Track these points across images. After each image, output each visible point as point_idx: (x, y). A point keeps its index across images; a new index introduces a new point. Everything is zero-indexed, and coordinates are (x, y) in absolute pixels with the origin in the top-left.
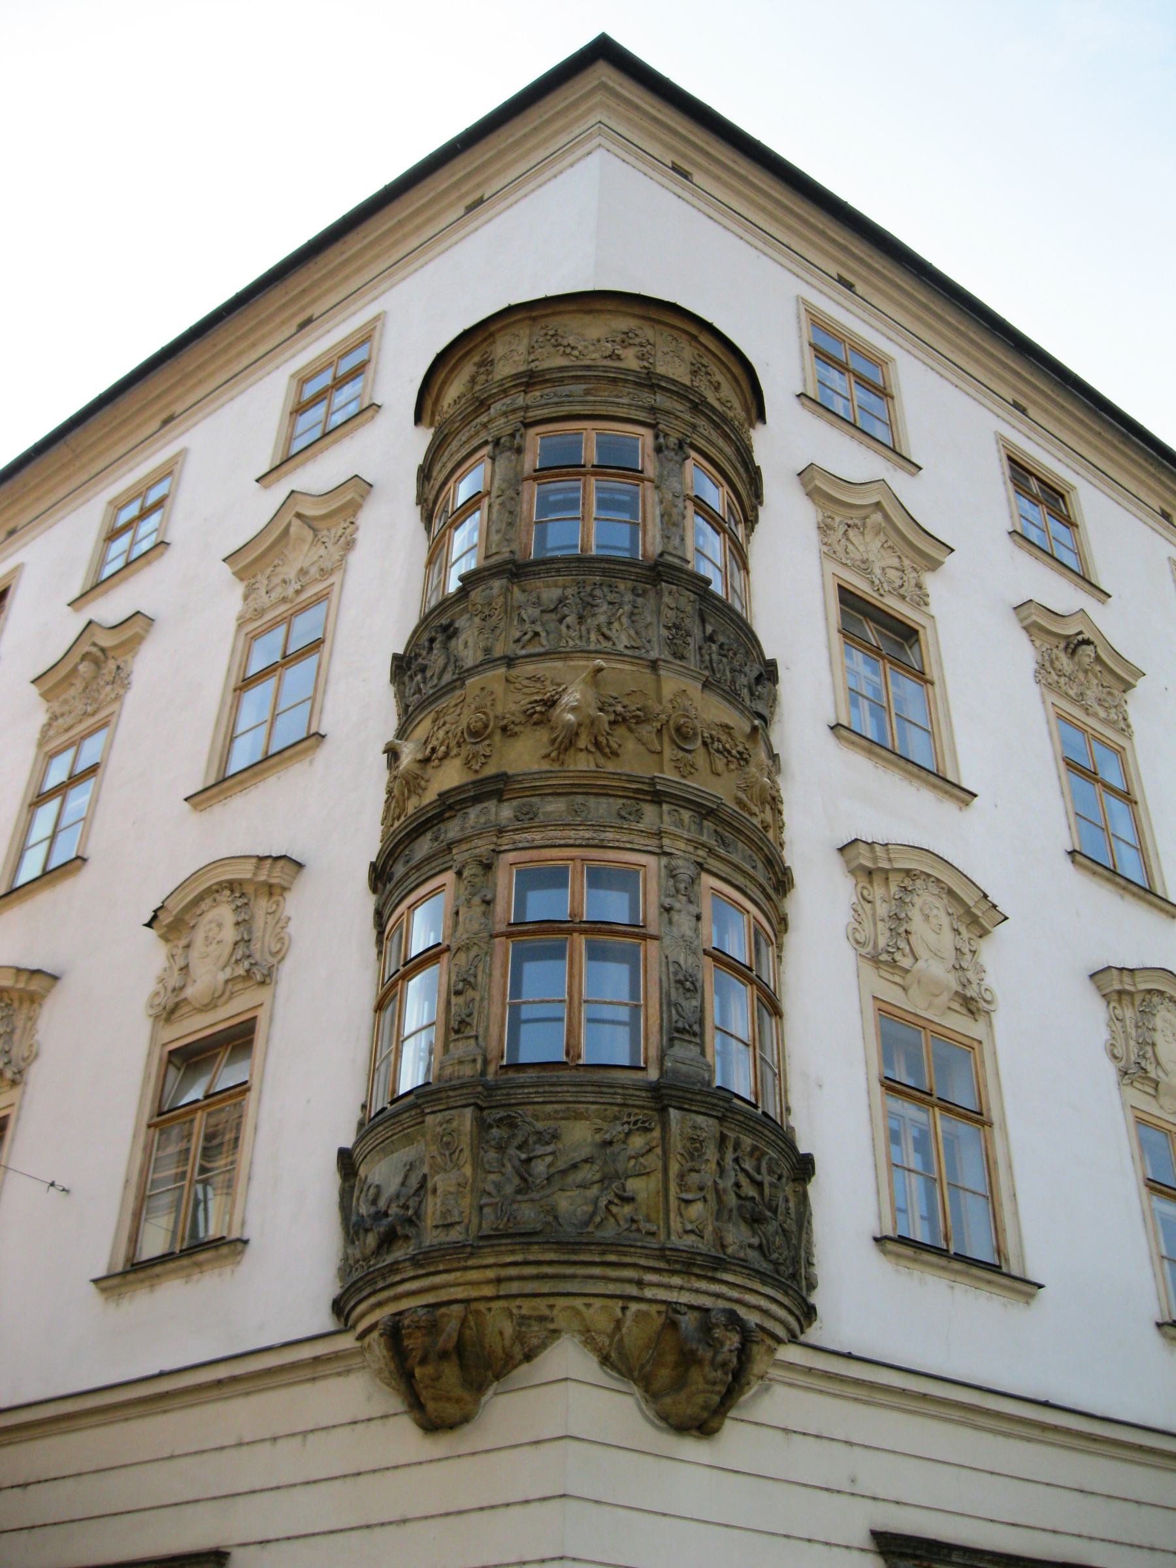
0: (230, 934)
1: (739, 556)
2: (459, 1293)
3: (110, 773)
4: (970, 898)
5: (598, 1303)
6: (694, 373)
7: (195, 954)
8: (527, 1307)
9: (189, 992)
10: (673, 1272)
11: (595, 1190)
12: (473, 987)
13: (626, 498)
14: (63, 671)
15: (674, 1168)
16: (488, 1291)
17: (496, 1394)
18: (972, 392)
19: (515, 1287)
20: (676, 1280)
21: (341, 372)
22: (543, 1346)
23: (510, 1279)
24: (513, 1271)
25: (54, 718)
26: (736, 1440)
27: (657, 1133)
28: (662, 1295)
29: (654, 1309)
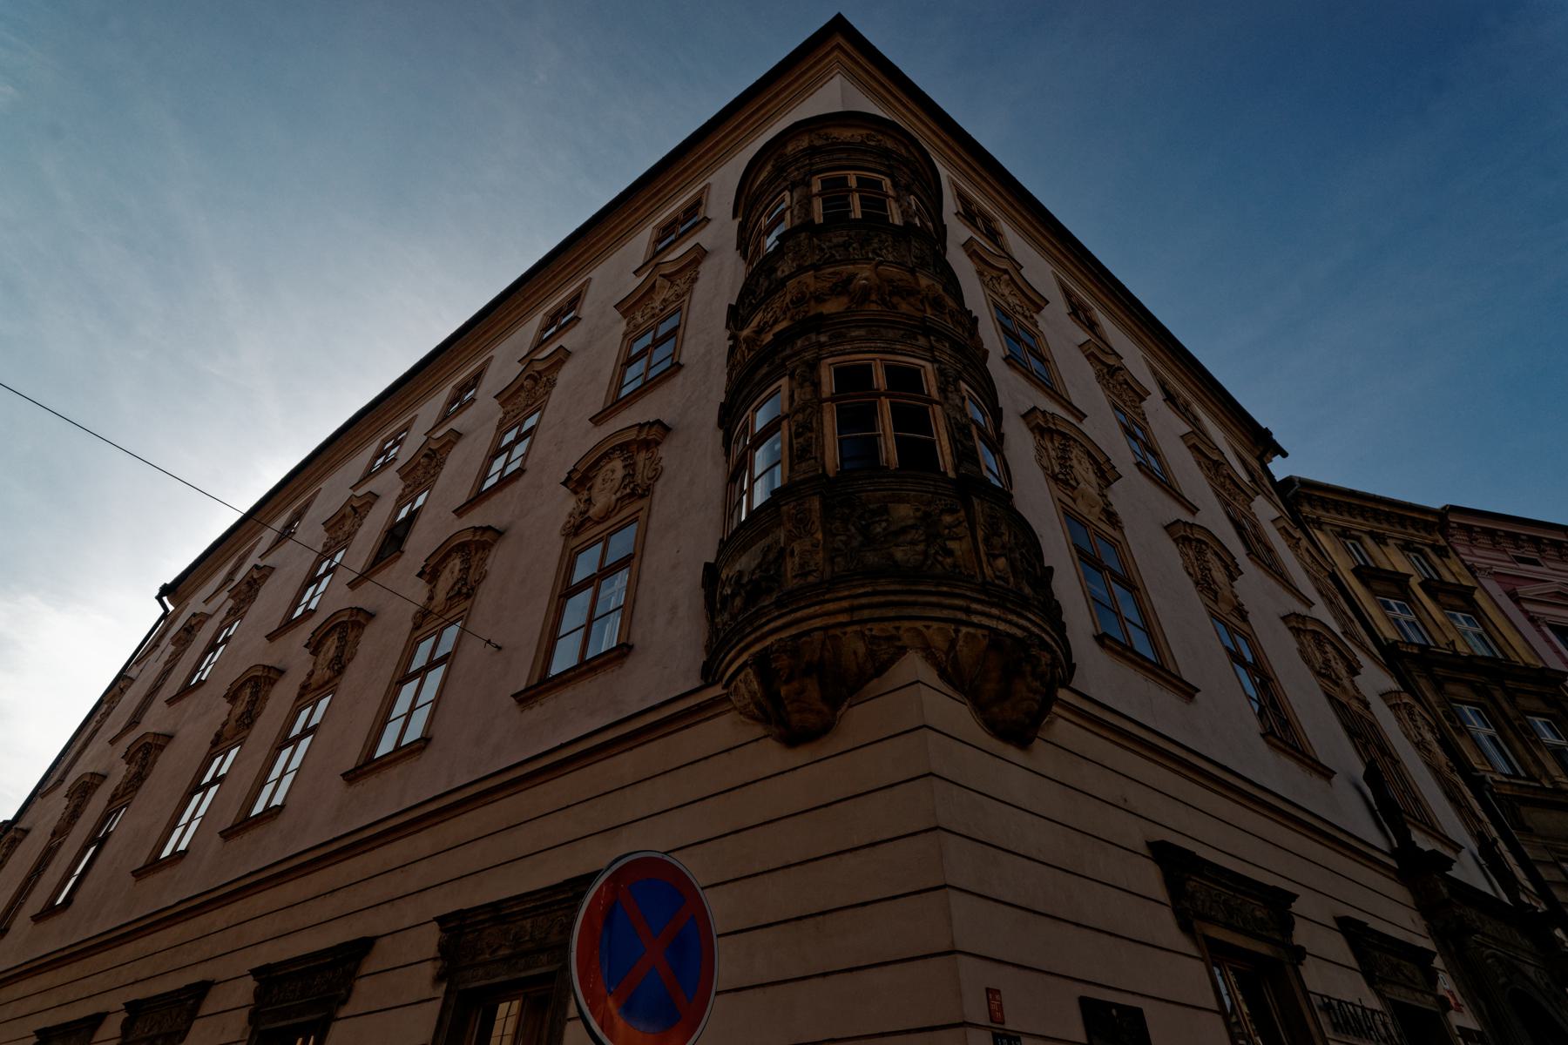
0: (620, 473)
2: (818, 623)
3: (541, 436)
4: (1101, 460)
5: (935, 625)
7: (595, 491)
8: (876, 629)
9: (591, 513)
10: (992, 605)
11: (921, 547)
12: (811, 430)
14: (513, 389)
15: (980, 534)
16: (842, 618)
17: (850, 706)
19: (866, 614)
20: (995, 611)
21: (659, 335)
22: (892, 661)
23: (862, 607)
24: (864, 601)
25: (506, 414)
26: (1042, 755)
27: (962, 513)
28: (986, 621)
29: (980, 632)
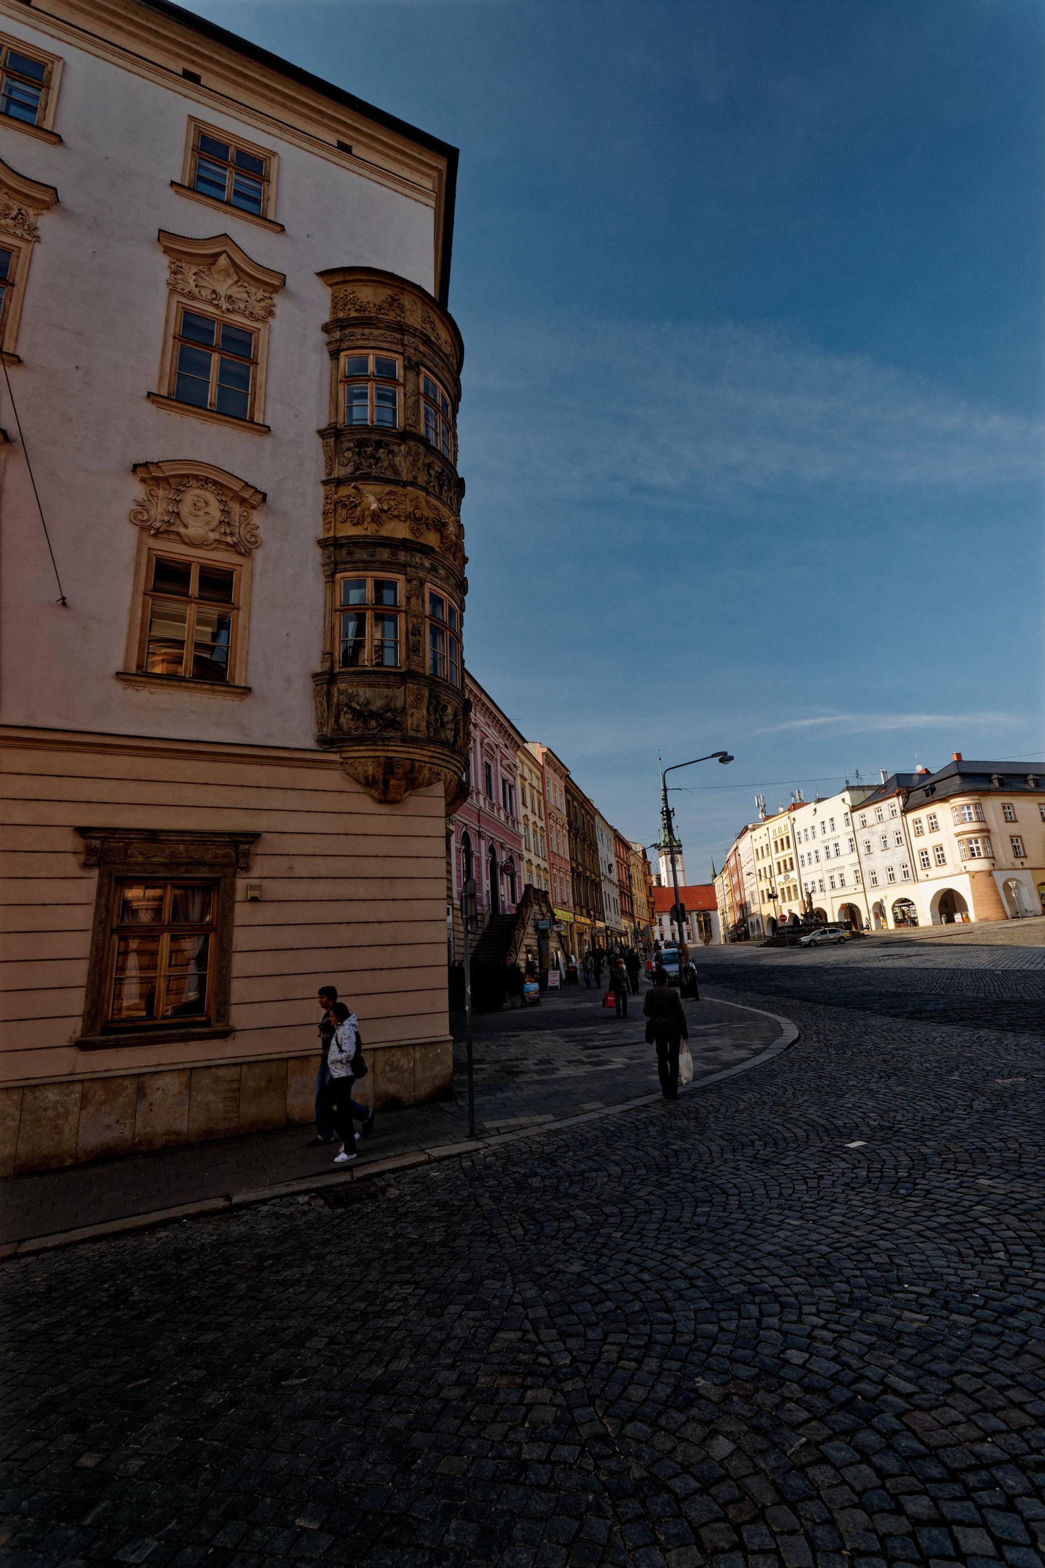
1: (451, 427)
6: (424, 321)
8: (436, 769)
13: (391, 394)
16: (427, 759)
18: (129, 66)
24: (437, 755)
